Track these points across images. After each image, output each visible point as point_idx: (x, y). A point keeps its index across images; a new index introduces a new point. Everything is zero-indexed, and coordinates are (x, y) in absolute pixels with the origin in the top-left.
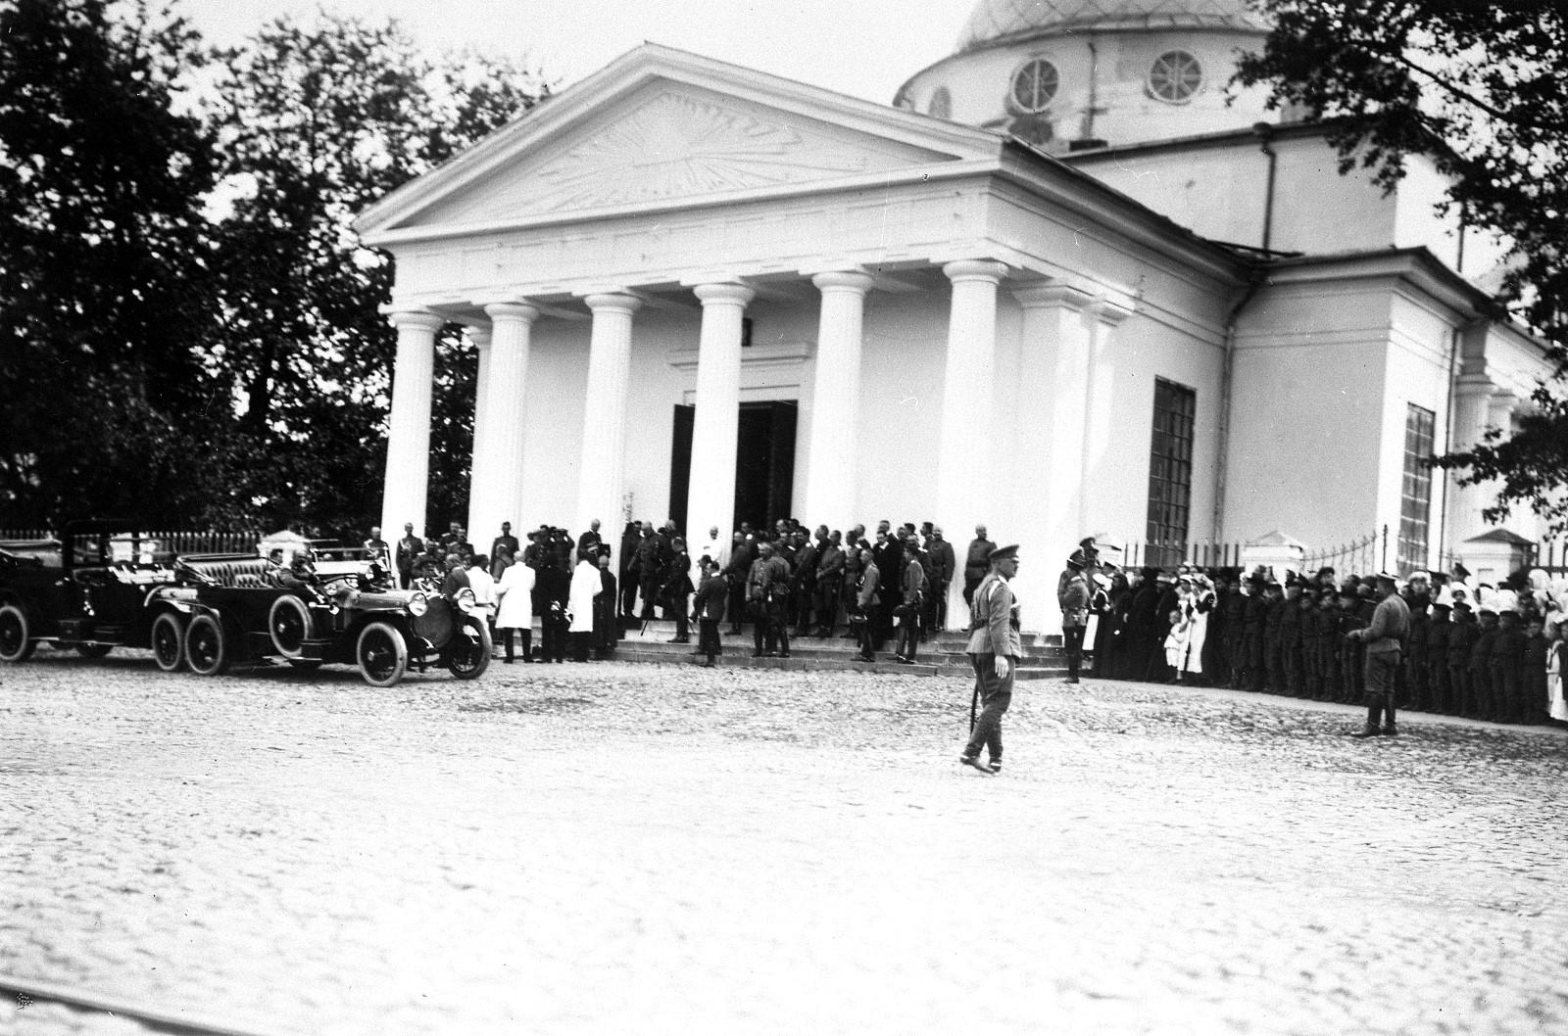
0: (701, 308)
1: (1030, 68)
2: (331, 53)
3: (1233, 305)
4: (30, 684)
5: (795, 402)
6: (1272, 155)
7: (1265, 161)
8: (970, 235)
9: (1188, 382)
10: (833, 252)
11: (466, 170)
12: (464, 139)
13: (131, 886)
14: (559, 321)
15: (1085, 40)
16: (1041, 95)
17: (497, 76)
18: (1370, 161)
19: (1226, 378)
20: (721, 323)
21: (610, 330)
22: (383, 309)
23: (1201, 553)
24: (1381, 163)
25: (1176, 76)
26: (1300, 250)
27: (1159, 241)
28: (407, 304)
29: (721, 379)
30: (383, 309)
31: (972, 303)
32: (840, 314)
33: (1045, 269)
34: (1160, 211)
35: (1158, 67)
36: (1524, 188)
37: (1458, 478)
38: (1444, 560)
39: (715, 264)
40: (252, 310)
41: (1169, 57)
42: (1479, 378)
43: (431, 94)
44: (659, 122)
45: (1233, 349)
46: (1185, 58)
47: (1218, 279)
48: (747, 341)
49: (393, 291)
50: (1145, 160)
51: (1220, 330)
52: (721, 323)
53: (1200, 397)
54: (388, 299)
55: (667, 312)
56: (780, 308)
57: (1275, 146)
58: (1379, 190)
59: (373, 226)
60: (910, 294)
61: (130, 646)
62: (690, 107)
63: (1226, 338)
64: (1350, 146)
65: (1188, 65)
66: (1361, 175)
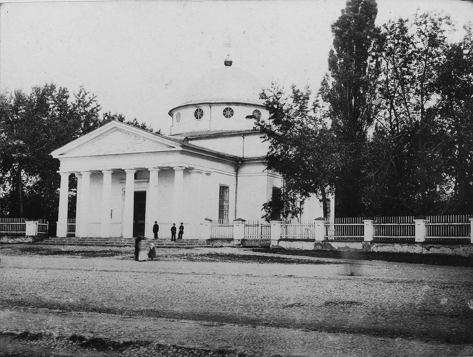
1: (197, 110)
10: (152, 164)
13: (289, 279)
14: (97, 175)
16: (200, 116)
20: (130, 177)
21: (107, 177)
22: (58, 172)
26: (327, 60)
28: (64, 172)
29: (131, 185)
30: (58, 172)
31: (179, 174)
32: (154, 176)
36: (72, 342)
39: (130, 165)
43: (68, 195)
48: (135, 178)
52: (130, 177)
53: (230, 189)
56: (141, 174)
60: (166, 172)
62: (129, 136)
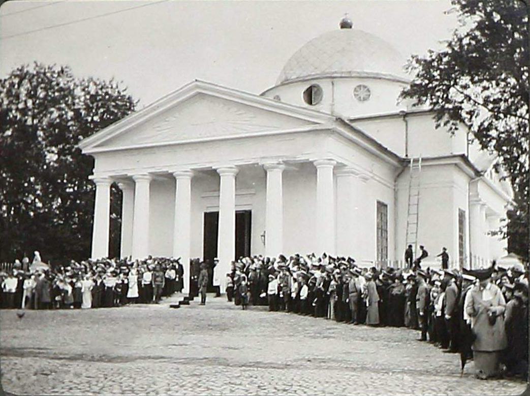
0: (220, 177)
2: (43, 79)
3: (397, 174)
4: (214, 366)
5: (250, 212)
6: (406, 122)
7: (404, 124)
9: (386, 202)
11: (130, 123)
12: (472, 109)
14: (164, 183)
15: (329, 80)
17: (101, 89)
18: (445, 124)
19: (396, 199)
23: (392, 263)
24: (449, 125)
25: (362, 93)
32: (275, 179)
33: (346, 163)
34: (379, 142)
35: (355, 90)
40: (523, 193)
41: (360, 86)
44: (202, 109)
45: (398, 190)
47: (393, 165)
49: (94, 171)
50: (370, 122)
51: (393, 183)
54: (92, 174)
55: (207, 179)
56: (252, 177)
57: (407, 118)
58: (450, 134)
59: (87, 146)
63: (395, 186)
64: (440, 118)
65: (366, 89)
66: (444, 129)
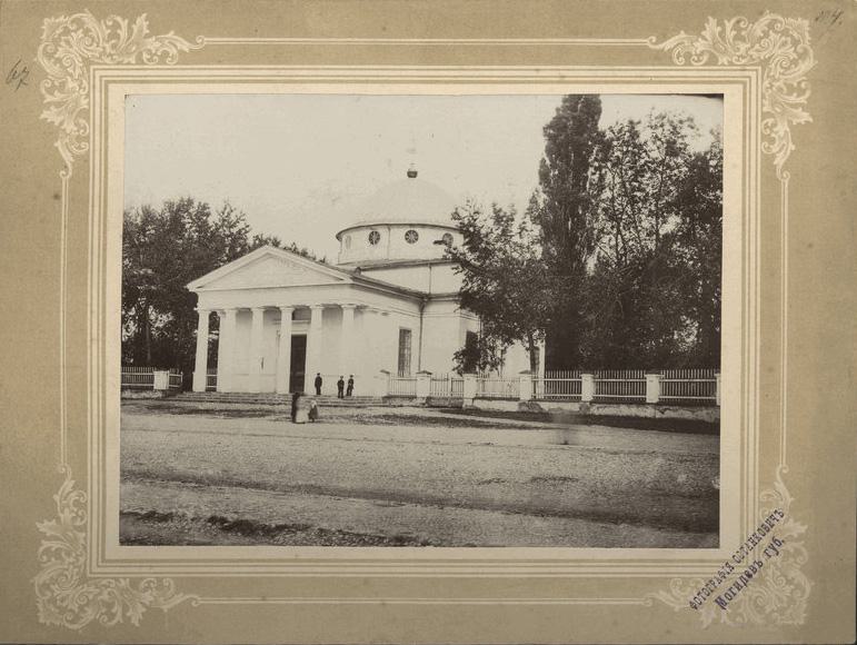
8: (347, 297)
10: (314, 300)
14: (244, 313)
20: (286, 316)
21: (258, 316)
25: (412, 237)
27: (400, 293)
29: (288, 328)
31: (348, 314)
32: (316, 315)
37: (306, 418)
38: (432, 512)
39: (286, 302)
42: (703, 414)
46: (414, 232)
52: (286, 316)
55: (272, 313)
56: (300, 313)
60: (332, 311)
61: (673, 419)
